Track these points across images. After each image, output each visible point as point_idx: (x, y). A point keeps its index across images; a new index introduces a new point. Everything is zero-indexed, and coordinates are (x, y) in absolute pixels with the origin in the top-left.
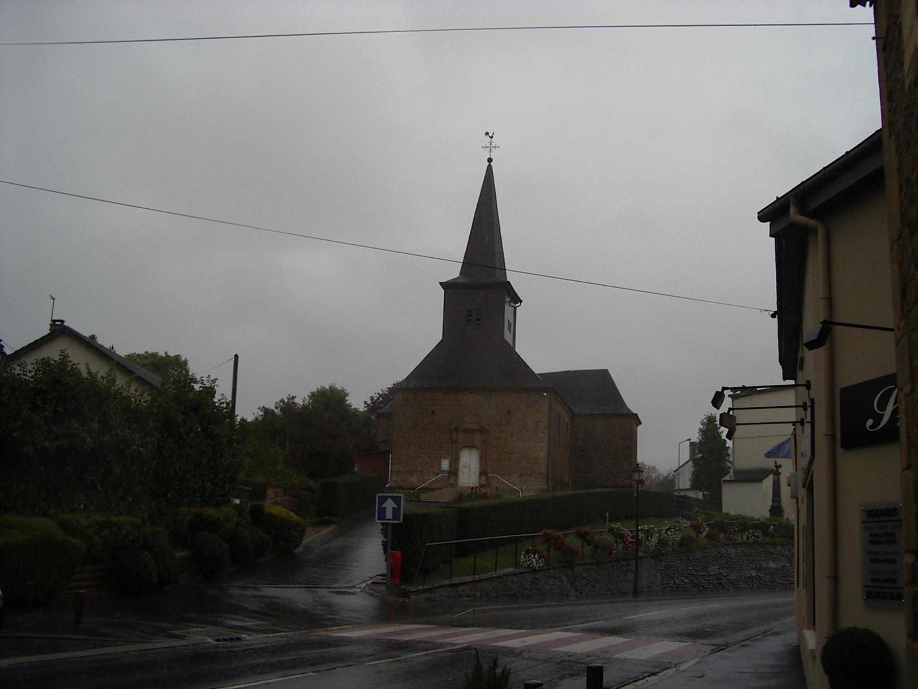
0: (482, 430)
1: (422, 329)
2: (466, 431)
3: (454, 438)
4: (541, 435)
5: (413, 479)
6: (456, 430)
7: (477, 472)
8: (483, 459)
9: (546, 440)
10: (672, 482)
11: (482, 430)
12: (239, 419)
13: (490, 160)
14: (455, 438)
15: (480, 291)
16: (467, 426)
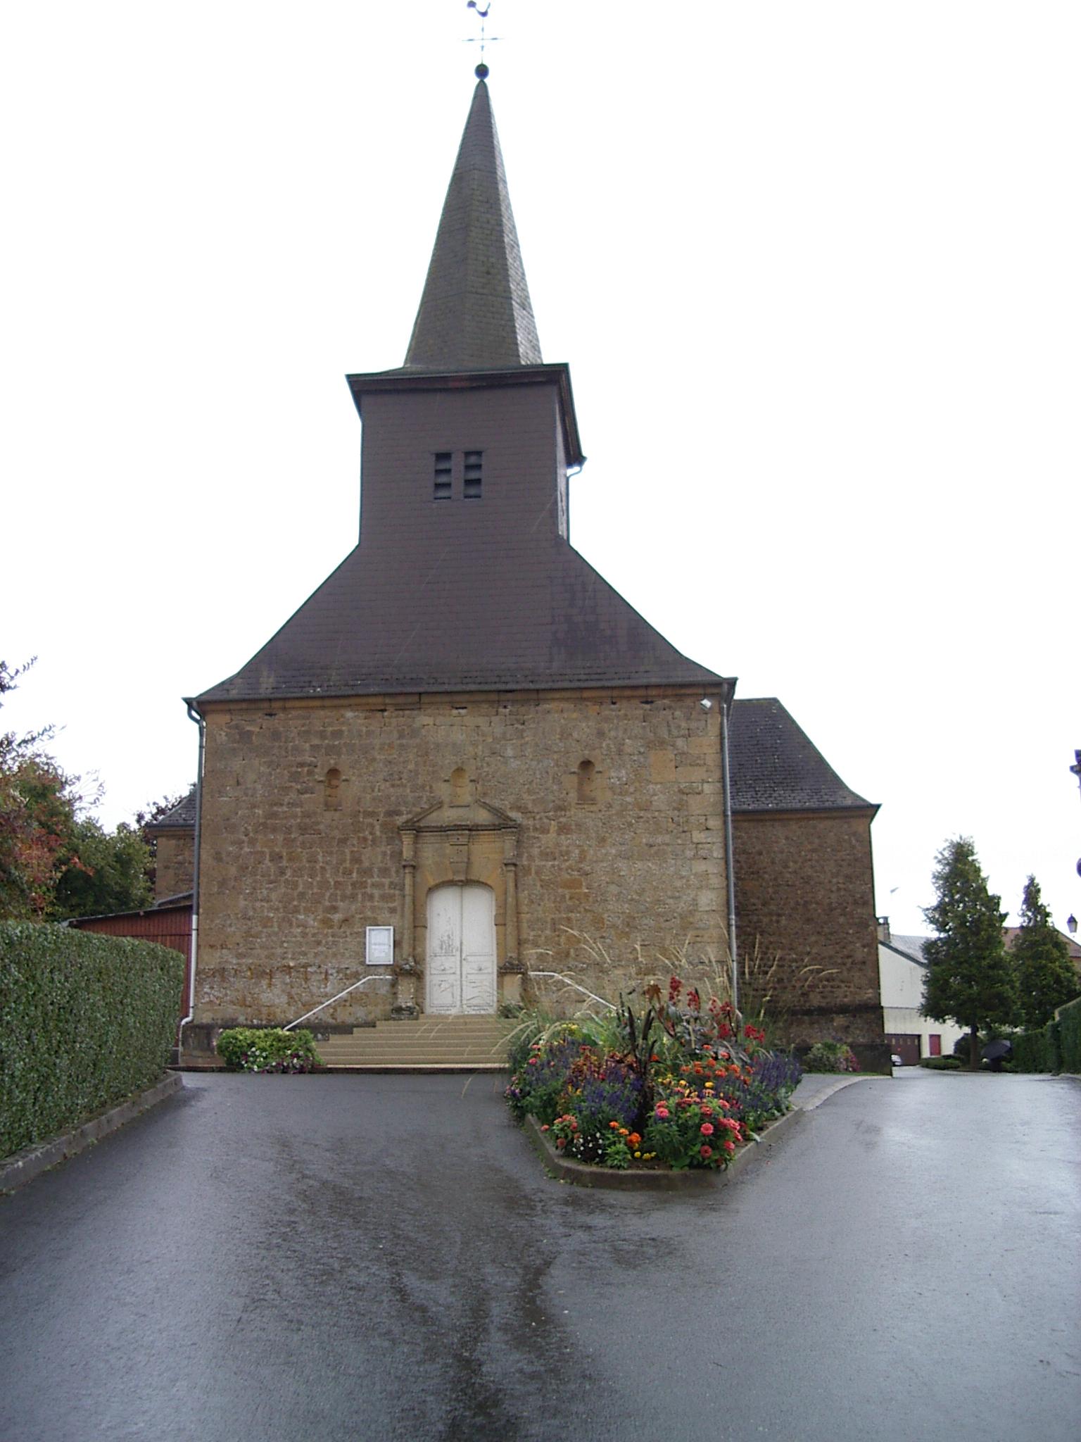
0: (503, 825)
1: (290, 520)
2: (443, 830)
3: (407, 853)
4: (698, 836)
5: (273, 996)
6: (417, 829)
7: (491, 966)
8: (508, 920)
9: (718, 853)
10: (63, 785)
11: (503, 825)
12: (905, 901)
13: (482, 71)
14: (413, 853)
15: (468, 413)
16: (448, 816)
